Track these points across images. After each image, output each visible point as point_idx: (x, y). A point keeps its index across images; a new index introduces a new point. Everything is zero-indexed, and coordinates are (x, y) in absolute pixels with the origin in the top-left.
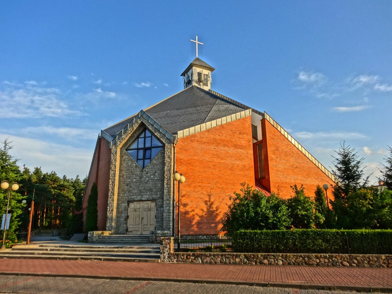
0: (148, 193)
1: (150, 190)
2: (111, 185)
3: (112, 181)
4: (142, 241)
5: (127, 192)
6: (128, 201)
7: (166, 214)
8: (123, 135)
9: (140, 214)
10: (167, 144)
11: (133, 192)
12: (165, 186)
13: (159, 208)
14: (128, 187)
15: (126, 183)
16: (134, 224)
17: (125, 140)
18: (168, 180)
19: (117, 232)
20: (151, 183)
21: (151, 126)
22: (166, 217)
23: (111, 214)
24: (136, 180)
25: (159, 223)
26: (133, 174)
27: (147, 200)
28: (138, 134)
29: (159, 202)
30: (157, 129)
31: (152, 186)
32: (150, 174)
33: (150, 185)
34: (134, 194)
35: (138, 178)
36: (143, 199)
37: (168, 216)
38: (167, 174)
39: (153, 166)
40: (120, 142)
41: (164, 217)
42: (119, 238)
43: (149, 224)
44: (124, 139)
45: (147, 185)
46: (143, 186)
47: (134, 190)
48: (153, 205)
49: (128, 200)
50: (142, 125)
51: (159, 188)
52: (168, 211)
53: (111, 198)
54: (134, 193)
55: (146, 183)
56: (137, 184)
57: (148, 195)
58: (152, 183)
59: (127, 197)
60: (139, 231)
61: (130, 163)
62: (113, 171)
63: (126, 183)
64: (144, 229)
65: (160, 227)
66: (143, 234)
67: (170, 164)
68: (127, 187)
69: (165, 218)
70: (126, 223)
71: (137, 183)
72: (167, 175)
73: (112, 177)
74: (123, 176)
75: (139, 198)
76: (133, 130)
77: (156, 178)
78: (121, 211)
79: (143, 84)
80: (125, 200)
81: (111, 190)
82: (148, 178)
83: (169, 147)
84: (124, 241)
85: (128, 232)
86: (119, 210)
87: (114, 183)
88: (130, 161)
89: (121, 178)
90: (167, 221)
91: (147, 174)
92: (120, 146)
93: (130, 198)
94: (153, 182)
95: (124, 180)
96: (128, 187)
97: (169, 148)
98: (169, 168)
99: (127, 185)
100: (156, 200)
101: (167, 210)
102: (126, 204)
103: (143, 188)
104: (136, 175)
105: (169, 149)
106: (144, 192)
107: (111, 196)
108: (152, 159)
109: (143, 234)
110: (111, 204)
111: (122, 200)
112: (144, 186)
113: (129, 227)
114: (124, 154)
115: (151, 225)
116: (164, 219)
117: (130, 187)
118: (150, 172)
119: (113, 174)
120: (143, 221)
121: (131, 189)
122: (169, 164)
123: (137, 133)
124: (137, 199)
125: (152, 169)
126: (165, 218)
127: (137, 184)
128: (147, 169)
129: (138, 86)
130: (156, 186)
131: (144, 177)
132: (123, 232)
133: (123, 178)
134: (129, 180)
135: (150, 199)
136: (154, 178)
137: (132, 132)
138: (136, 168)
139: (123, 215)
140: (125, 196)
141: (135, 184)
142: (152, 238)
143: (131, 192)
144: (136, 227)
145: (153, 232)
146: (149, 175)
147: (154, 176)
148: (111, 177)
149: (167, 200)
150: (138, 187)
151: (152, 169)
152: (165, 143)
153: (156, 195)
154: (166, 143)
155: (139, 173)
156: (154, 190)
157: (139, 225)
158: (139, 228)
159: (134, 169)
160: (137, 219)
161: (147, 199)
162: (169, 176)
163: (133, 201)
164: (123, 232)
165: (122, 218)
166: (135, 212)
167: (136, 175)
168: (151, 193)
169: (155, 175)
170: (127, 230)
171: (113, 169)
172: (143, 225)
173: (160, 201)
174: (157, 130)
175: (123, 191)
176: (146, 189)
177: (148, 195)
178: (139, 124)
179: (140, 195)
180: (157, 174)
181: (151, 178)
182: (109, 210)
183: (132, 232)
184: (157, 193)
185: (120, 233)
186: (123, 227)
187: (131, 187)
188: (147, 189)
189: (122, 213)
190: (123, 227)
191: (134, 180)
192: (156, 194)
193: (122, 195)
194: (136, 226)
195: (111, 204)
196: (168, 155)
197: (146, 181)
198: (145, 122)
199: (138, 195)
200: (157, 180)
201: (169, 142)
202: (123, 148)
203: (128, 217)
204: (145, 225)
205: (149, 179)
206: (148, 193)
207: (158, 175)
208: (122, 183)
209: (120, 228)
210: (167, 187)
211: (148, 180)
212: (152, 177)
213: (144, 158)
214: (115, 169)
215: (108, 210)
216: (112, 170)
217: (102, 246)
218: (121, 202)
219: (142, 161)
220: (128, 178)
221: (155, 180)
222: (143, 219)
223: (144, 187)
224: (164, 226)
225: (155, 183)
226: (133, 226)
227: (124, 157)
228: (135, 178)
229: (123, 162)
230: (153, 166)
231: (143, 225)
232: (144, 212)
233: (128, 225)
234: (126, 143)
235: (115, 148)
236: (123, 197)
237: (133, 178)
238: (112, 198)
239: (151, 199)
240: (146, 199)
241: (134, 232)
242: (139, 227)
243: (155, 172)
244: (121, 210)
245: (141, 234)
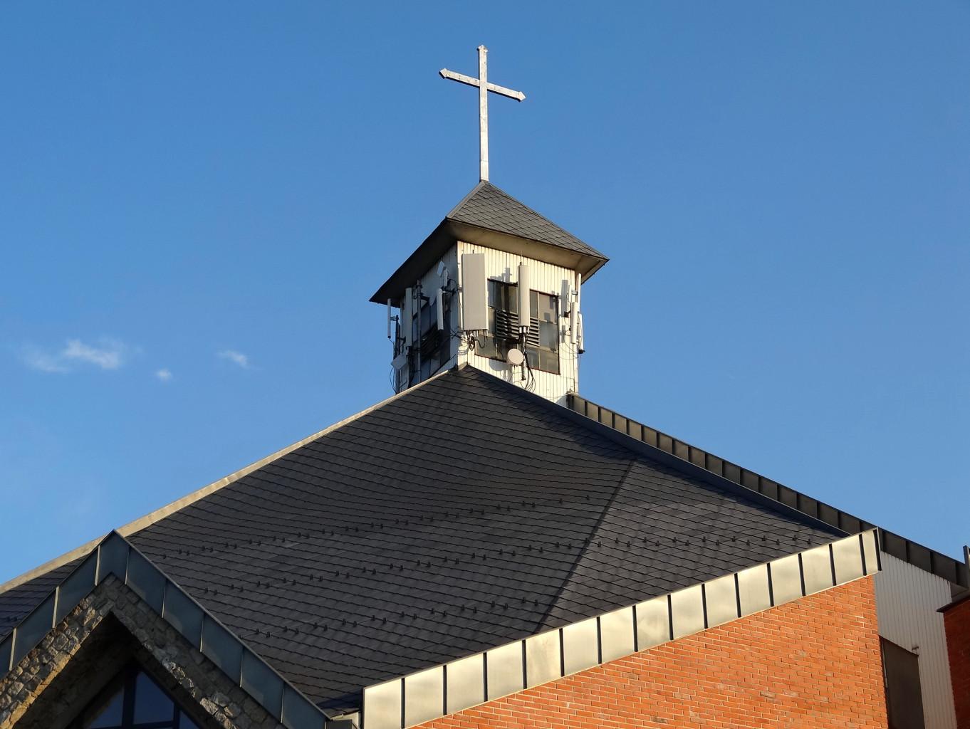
21: (174, 651)
79: (76, 350)
137: (40, 688)
174: (214, 676)
178: (87, 634)
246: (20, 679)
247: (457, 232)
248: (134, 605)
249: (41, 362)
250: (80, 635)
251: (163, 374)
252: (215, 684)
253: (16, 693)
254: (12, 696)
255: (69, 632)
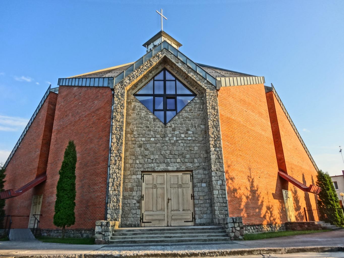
0: (179, 160)
1: (182, 155)
2: (116, 144)
3: (117, 138)
4: (208, 236)
5: (140, 157)
6: (142, 172)
7: (217, 192)
8: (135, 71)
9: (164, 194)
10: (208, 90)
11: (152, 157)
12: (212, 149)
13: (199, 183)
14: (143, 149)
15: (137, 143)
16: (154, 209)
17: (138, 78)
18: (215, 141)
19: (123, 223)
20: (182, 144)
21: (181, 64)
22: (218, 196)
23: (117, 192)
24: (156, 139)
25: (200, 207)
26: (150, 130)
27: (177, 171)
28: (154, 75)
29: (198, 173)
30: (190, 68)
31: (183, 149)
32: (179, 132)
33: (181, 147)
34: (154, 161)
35: (159, 136)
36: (170, 168)
37: (222, 194)
38: (214, 132)
39: (183, 121)
40: (130, 80)
41: (215, 196)
42: (151, 232)
43: (181, 210)
44: (137, 76)
45: (175, 148)
46: (168, 150)
47: (153, 154)
48: (187, 177)
49: (142, 170)
50: (165, 60)
51: (196, 153)
52: (221, 187)
53: (115, 164)
54: (153, 160)
55: (173, 144)
56: (158, 146)
57: (178, 163)
58: (184, 145)
59: (141, 166)
60: (164, 220)
61: (143, 114)
62: (119, 122)
63: (137, 143)
64: (173, 217)
65: (204, 213)
66: (171, 226)
67: (216, 117)
68: (140, 150)
69: (217, 197)
70: (140, 208)
71: (157, 143)
72: (213, 134)
73: (116, 132)
74: (133, 132)
75: (162, 167)
76: (151, 65)
77: (189, 138)
78: (130, 188)
79: (23, 78)
80: (137, 170)
81: (115, 152)
82: (176, 137)
83: (212, 94)
84: (172, 239)
85: (143, 222)
86: (127, 185)
87: (121, 141)
88: (144, 111)
89: (129, 135)
90: (220, 203)
91: (174, 131)
92: (128, 87)
93: (145, 166)
94: (185, 145)
95: (133, 139)
96: (143, 149)
97: (212, 96)
98: (216, 124)
99: (140, 146)
100: (192, 171)
101: (219, 187)
102: (139, 177)
103: (168, 152)
104: (155, 131)
105: (213, 97)
106: (171, 159)
107: (116, 161)
108: (179, 110)
109: (172, 225)
110: (115, 174)
111: (132, 169)
112: (170, 149)
113: (145, 213)
114: (133, 100)
115: (183, 210)
116: (216, 200)
117: (146, 150)
118: (179, 129)
119: (118, 126)
120: (169, 204)
121: (147, 153)
122: (215, 118)
123: (153, 72)
124: (159, 169)
125: (181, 124)
126: (217, 197)
127: (158, 145)
128: (174, 124)
129: (17, 79)
130: (191, 150)
131: (170, 135)
132: (137, 222)
133: (132, 136)
134: (143, 139)
135: (182, 170)
136: (186, 138)
137: (150, 68)
138: (154, 121)
139: (134, 193)
140: (138, 164)
141: (154, 145)
142: (234, 231)
143: (147, 157)
144: (157, 215)
145: (235, 220)
146: (177, 132)
147: (186, 135)
148: (114, 131)
149: (217, 171)
150: (160, 150)
151: (181, 124)
152: (205, 88)
153: (191, 163)
154: (207, 89)
155: (160, 129)
156: (188, 156)
157: (164, 210)
158: (165, 217)
159: (150, 123)
160: (160, 200)
161: (177, 168)
162: (217, 135)
163: (150, 172)
164: (137, 222)
165: (133, 199)
166: (155, 190)
167: (155, 131)
168: (184, 160)
169: (187, 133)
170: (142, 219)
171: (118, 120)
172: (170, 210)
173: (199, 172)
174: (190, 70)
175: (134, 155)
176: (173, 153)
177: (178, 163)
178: (160, 59)
179: (164, 163)
180: (190, 132)
181: (181, 138)
182: (113, 184)
183: (151, 222)
184: (194, 160)
185: (129, 224)
186: (136, 213)
187: (147, 149)
188: (176, 153)
189: (132, 190)
190: (136, 213)
191: (152, 139)
192: (193, 162)
193: (131, 161)
194: (158, 213)
195: (115, 174)
196: (212, 106)
197: (172, 142)
198: (171, 57)
199: (161, 163)
200: (192, 141)
201: (212, 88)
202: (131, 91)
203: (142, 197)
204: (174, 210)
205: (178, 139)
206: (179, 160)
207: (193, 133)
208: (130, 143)
209: (129, 216)
210: (215, 150)
211: (177, 141)
212: (183, 136)
213: (165, 110)
214: (121, 120)
215: (111, 185)
216: (117, 120)
217: (224, 248)
218: (129, 172)
219: (162, 113)
220: (141, 136)
221: (188, 142)
222: (170, 201)
223: (170, 151)
224: (216, 211)
225: (189, 145)
226: (151, 213)
227: (133, 104)
228: (154, 136)
229: (131, 111)
230: (183, 121)
231: (170, 210)
232: (172, 190)
233: (143, 212)
234: (136, 85)
235: (121, 88)
236: (133, 165)
237: (150, 136)
238: (117, 164)
239: (184, 170)
240: (175, 169)
241: (154, 222)
242: (164, 213)
243: (188, 130)
244: (129, 185)
245: (168, 226)
246: (145, 66)
247: (162, 34)
248: (171, 55)
249: (17, 79)
250: (159, 60)
251: (38, 83)
252: (190, 71)
253: (145, 69)
254: (144, 69)
255: (156, 58)
